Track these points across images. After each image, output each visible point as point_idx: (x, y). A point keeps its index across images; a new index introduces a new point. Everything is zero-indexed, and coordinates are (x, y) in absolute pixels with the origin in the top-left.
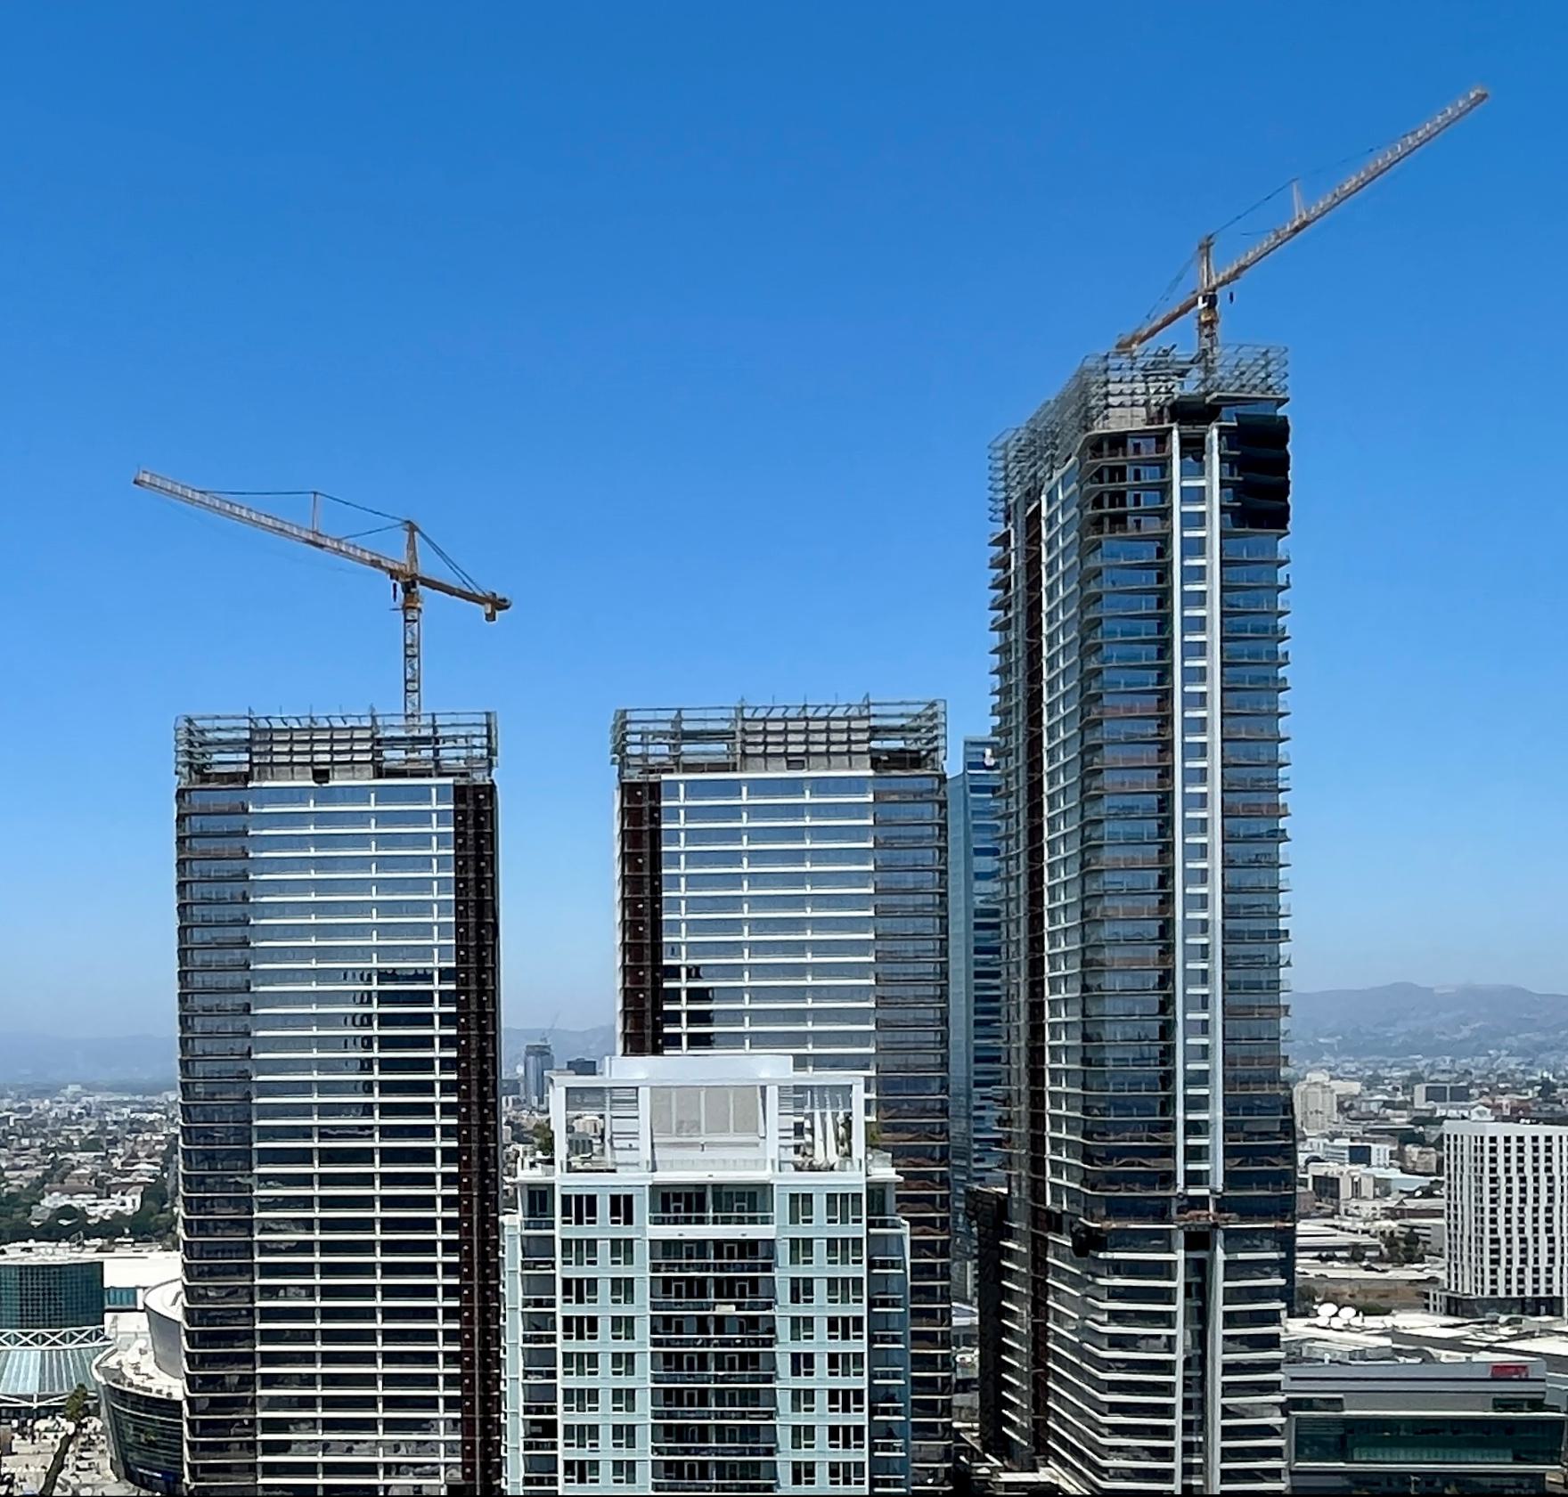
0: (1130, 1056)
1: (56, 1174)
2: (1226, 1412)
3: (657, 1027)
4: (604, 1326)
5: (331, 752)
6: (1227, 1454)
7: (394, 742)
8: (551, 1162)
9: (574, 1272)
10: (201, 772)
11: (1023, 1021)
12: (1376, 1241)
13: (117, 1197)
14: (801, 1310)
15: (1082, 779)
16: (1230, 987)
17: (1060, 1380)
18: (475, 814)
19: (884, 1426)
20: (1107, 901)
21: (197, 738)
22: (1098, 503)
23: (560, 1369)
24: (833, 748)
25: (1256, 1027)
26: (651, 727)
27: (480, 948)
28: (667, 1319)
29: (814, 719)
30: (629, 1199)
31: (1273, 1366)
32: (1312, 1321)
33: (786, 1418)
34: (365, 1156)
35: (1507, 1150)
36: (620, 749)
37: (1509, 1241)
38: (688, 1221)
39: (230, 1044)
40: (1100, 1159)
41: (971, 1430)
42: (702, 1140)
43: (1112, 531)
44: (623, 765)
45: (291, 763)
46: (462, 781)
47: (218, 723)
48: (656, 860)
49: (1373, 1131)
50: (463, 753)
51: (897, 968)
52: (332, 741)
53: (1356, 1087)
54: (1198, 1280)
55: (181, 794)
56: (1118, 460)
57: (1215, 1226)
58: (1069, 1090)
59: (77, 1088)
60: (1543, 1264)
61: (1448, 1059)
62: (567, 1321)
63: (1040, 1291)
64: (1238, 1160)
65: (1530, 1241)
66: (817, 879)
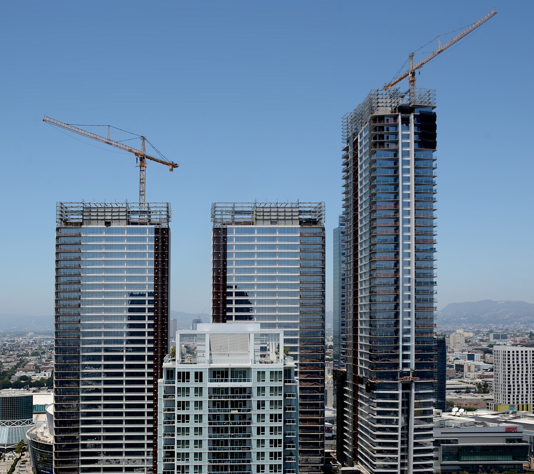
0: (385, 324)
1: (21, 364)
2: (416, 444)
3: (224, 313)
4: (192, 418)
5: (112, 216)
6: (415, 459)
7: (134, 212)
8: (174, 360)
9: (182, 399)
10: (66, 222)
11: (351, 312)
12: (475, 386)
13: (43, 373)
14: (261, 412)
15: (370, 230)
16: (417, 301)
17: (362, 435)
18: (162, 238)
19: (289, 452)
20: (377, 271)
21: (65, 209)
22: (375, 138)
23: (176, 433)
24: (287, 218)
25: (426, 314)
26: (224, 209)
27: (163, 285)
28: (214, 415)
29: (280, 208)
30: (201, 373)
31: (431, 429)
32: (450, 413)
33: (255, 449)
34: (120, 358)
35: (513, 355)
36: (213, 216)
37: (514, 386)
38: (222, 381)
39: (72, 318)
40: (374, 359)
41: (334, 452)
42: (228, 353)
43: (380, 148)
44: (215, 222)
45: (98, 219)
46: (158, 227)
47: (72, 205)
48: (225, 255)
49: (476, 349)
50: (158, 217)
51: (307, 293)
52: (112, 212)
53: (471, 335)
54: (407, 400)
55: (58, 229)
56: (382, 124)
57: (412, 381)
58: (365, 335)
59: (32, 333)
60: (525, 393)
61: (502, 325)
62: (179, 416)
63: (356, 404)
64: (419, 359)
65: (521, 386)
66: (280, 262)
